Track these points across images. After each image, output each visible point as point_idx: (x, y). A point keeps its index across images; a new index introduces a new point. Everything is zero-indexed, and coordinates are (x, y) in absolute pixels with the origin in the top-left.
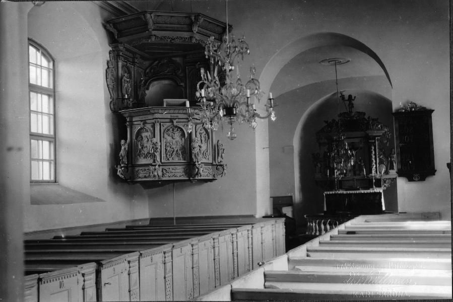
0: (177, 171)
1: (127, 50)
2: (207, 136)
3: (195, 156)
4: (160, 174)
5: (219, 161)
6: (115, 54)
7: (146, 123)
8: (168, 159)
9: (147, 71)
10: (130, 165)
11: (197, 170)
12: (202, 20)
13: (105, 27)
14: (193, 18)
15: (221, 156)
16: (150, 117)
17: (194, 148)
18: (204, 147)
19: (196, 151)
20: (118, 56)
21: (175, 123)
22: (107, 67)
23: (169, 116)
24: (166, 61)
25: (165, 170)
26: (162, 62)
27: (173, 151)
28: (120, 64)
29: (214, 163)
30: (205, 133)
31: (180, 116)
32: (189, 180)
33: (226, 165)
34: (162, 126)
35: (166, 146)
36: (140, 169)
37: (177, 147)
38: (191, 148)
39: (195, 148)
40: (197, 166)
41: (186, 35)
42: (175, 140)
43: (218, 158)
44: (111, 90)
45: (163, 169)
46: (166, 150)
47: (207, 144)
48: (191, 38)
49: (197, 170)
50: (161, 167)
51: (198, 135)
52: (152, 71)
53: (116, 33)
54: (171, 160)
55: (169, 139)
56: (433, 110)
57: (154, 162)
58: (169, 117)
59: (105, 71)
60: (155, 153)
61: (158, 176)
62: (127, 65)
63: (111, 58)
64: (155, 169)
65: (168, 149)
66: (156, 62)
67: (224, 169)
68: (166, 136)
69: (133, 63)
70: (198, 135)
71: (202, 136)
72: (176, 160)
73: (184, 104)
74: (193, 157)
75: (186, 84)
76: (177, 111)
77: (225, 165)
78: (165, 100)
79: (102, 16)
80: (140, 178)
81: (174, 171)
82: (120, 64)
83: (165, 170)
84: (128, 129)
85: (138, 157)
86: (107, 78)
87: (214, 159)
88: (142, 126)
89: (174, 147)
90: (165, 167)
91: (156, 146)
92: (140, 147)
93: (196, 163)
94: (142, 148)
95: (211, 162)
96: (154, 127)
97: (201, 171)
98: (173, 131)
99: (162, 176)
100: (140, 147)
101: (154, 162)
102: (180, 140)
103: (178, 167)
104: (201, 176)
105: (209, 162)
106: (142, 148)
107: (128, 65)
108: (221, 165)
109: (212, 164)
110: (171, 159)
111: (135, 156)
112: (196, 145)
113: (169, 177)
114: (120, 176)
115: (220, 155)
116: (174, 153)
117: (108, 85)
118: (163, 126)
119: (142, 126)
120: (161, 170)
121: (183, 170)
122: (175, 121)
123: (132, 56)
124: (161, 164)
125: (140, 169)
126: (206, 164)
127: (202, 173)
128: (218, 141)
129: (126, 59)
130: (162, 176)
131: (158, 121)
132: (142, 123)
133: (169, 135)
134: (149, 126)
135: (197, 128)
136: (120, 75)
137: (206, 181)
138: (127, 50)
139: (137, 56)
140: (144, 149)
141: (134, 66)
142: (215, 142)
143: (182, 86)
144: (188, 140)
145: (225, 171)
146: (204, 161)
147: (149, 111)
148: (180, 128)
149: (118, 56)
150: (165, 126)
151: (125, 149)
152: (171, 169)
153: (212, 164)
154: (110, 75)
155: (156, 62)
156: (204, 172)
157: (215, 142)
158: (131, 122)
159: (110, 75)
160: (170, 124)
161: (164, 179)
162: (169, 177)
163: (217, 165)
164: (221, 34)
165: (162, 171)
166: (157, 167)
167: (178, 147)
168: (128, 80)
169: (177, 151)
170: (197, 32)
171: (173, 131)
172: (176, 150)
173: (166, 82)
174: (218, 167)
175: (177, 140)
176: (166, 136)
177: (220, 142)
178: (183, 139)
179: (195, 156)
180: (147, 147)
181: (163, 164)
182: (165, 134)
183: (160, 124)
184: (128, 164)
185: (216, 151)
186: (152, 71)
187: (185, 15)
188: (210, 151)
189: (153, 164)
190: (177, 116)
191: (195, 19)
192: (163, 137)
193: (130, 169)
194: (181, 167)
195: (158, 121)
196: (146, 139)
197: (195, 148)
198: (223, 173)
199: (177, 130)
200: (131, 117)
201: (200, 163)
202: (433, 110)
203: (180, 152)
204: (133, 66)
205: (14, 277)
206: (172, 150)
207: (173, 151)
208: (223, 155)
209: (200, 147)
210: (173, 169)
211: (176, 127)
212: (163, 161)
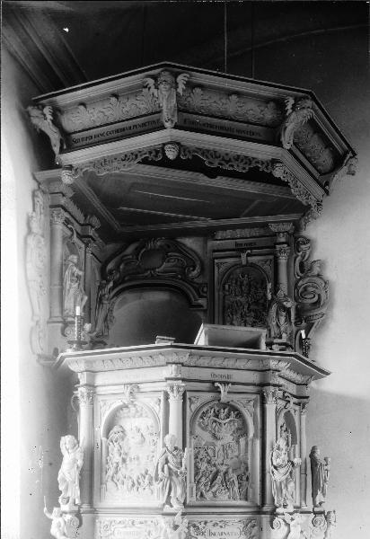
8: (202, 495)
9: (110, 266)
21: (224, 397)
23: (205, 374)
24: (159, 243)
25: (194, 526)
26: (150, 245)
31: (238, 376)
36: (119, 519)
52: (121, 267)
53: (55, 137)
55: (206, 437)
56: (328, 374)
58: (210, 378)
65: (203, 466)
68: (198, 430)
73: (254, 344)
76: (230, 363)
83: (194, 526)
88: (126, 399)
90: (197, 519)
92: (116, 458)
94: (124, 461)
98: (217, 416)
102: (233, 444)
110: (209, 495)
116: (220, 478)
119: (126, 399)
123: (82, 222)
125: (119, 519)
139: (95, 221)
140: (132, 465)
141: (87, 245)
143: (202, 306)
145: (331, 527)
148: (234, 409)
151: (75, 461)
152: (210, 525)
158: (91, 386)
160: (209, 396)
169: (226, 473)
172: (223, 468)
173: (159, 297)
176: (198, 430)
180: (138, 458)
192: (191, 433)
193: (85, 517)
196: (138, 438)
199: (228, 416)
200: (92, 373)
202: (328, 374)
205: (67, 30)
206: (214, 469)
211: (226, 405)
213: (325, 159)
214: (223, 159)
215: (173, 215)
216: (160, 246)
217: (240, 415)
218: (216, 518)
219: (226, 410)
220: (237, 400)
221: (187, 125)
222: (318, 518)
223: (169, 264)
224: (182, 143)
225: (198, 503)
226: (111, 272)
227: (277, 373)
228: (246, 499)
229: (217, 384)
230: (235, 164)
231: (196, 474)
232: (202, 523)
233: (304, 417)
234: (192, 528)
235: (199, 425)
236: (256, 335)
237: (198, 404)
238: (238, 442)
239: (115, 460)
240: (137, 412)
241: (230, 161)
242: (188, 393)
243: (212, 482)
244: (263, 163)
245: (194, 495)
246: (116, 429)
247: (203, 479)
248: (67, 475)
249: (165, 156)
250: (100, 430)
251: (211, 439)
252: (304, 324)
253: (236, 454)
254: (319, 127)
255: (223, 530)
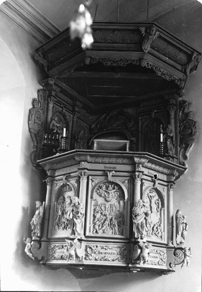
0: (109, 251)
1: (63, 91)
2: (160, 203)
3: (138, 228)
4: (81, 253)
5: (178, 242)
6: (46, 92)
7: (70, 177)
8: (97, 232)
10: (44, 239)
11: (139, 251)
12: (155, 34)
13: (33, 58)
14: (143, 30)
15: (182, 235)
16: (75, 168)
17: (136, 216)
18: (154, 218)
19: (140, 220)
20: (50, 96)
21: (110, 178)
22: (31, 107)
23: (101, 167)
25: (90, 248)
27: (105, 220)
28: (51, 106)
29: (171, 245)
30: (157, 197)
32: (125, 269)
33: (189, 249)
34: (90, 181)
35: (95, 210)
37: (110, 214)
38: (132, 215)
39: (138, 215)
40: (141, 244)
41: (134, 56)
42: (109, 203)
43: (176, 237)
44: (33, 135)
45: (86, 246)
46: (94, 216)
47: (161, 215)
48: (141, 59)
49: (139, 251)
50: (84, 244)
51: (146, 199)
52: (98, 126)
54: (100, 234)
55: (101, 200)
57: (73, 233)
59: (28, 112)
60: (75, 219)
61: (77, 256)
62: (62, 111)
63: (40, 99)
64: (72, 245)
65: (98, 216)
66: (104, 116)
67: (185, 255)
68: (95, 195)
69: (73, 112)
70: (146, 199)
71: (153, 201)
72: (109, 233)
74: (135, 230)
75: (138, 139)
77: (187, 249)
78: (96, 141)
79: (31, 46)
80: (55, 259)
81: (103, 251)
82: (51, 106)
83: (90, 248)
84: (48, 187)
85: (57, 226)
86: (29, 120)
87: (171, 238)
89: (107, 213)
90: (91, 244)
91: (77, 208)
93: (139, 240)
95: (166, 243)
96: (78, 182)
97: (145, 253)
98: (107, 189)
99: (85, 259)
100: (60, 213)
101: (73, 233)
102: (117, 204)
103: (111, 245)
104: (144, 262)
105: (162, 242)
106: (63, 214)
107: (64, 111)
108: (181, 249)
109: (166, 246)
111: (53, 226)
112: (140, 210)
113: (96, 260)
114: (28, 253)
115: (180, 233)
116: (107, 222)
117: (29, 129)
118: (92, 181)
120: (83, 247)
121: (118, 250)
122: (110, 175)
124: (84, 238)
126: (155, 244)
127: (147, 258)
128: (178, 211)
129: (57, 103)
130: (85, 259)
131: (85, 173)
132: (64, 178)
133: (100, 196)
134: (73, 182)
135: (144, 188)
136: (49, 119)
137: (162, 272)
138: (63, 91)
139: (78, 103)
141: (74, 115)
142: (172, 212)
144: (129, 203)
145: (187, 258)
146: (154, 239)
147: (73, 158)
149: (50, 96)
150: (96, 181)
151: (39, 214)
152: (99, 248)
153: (166, 246)
154: (33, 116)
155: (104, 116)
156: (152, 258)
157: (172, 212)
159: (33, 116)
161: (86, 262)
162: (96, 260)
163: (174, 248)
164: (184, 65)
165: (86, 250)
166: (76, 241)
167: (113, 214)
168: (58, 125)
169: (111, 220)
170: (148, 53)
171: (107, 189)
172: (109, 217)
174: (177, 252)
175: (112, 203)
176: (95, 195)
177: (180, 213)
178: (122, 202)
179: (138, 228)
181: (89, 239)
182: (95, 194)
183: (88, 178)
184: (41, 237)
185: (174, 225)
186: (98, 126)
187: (132, 28)
188: (165, 227)
189: (72, 237)
190: (114, 168)
191: (146, 31)
192: (92, 197)
194: (116, 245)
195: (85, 173)
196: (69, 201)
197: (138, 215)
198: (183, 261)
201: (145, 240)
203: (115, 222)
204: (72, 115)
207: (105, 220)
208: (185, 233)
209: (146, 214)
210: (102, 248)
211: (112, 183)
212: (87, 234)
213: (182, 57)
214: (113, 61)
215: (102, 96)
216: (116, 114)
217: (120, 188)
218: (104, 245)
219: (112, 186)
220: (118, 180)
221: (95, 48)
222: (178, 251)
223: (120, 122)
224: (92, 57)
225: (93, 235)
226: (93, 129)
227: (141, 165)
228: (122, 235)
229: (106, 172)
230: (119, 63)
231: (94, 220)
232: (95, 247)
233: (171, 193)
234: (88, 249)
235: (96, 191)
236: (123, 144)
237: (96, 182)
238: (119, 203)
239: (59, 214)
240: (69, 188)
241: (117, 61)
242: (90, 177)
243: (102, 224)
244: (134, 61)
245: (92, 231)
246: (61, 197)
247: (98, 222)
248: (35, 221)
249: (84, 64)
250: (54, 199)
251: (104, 202)
252: (184, 146)
253: (118, 209)
254: (113, 29)
255: (106, 251)
